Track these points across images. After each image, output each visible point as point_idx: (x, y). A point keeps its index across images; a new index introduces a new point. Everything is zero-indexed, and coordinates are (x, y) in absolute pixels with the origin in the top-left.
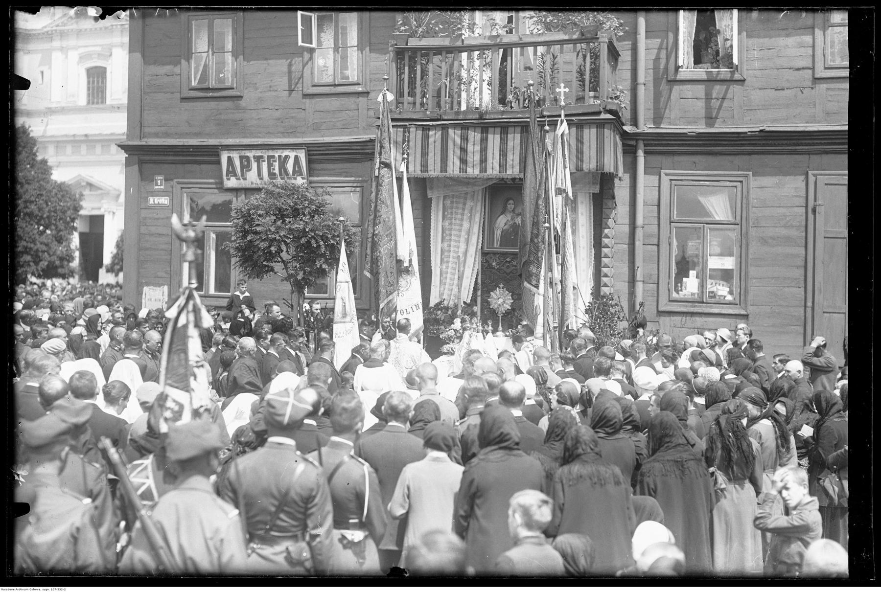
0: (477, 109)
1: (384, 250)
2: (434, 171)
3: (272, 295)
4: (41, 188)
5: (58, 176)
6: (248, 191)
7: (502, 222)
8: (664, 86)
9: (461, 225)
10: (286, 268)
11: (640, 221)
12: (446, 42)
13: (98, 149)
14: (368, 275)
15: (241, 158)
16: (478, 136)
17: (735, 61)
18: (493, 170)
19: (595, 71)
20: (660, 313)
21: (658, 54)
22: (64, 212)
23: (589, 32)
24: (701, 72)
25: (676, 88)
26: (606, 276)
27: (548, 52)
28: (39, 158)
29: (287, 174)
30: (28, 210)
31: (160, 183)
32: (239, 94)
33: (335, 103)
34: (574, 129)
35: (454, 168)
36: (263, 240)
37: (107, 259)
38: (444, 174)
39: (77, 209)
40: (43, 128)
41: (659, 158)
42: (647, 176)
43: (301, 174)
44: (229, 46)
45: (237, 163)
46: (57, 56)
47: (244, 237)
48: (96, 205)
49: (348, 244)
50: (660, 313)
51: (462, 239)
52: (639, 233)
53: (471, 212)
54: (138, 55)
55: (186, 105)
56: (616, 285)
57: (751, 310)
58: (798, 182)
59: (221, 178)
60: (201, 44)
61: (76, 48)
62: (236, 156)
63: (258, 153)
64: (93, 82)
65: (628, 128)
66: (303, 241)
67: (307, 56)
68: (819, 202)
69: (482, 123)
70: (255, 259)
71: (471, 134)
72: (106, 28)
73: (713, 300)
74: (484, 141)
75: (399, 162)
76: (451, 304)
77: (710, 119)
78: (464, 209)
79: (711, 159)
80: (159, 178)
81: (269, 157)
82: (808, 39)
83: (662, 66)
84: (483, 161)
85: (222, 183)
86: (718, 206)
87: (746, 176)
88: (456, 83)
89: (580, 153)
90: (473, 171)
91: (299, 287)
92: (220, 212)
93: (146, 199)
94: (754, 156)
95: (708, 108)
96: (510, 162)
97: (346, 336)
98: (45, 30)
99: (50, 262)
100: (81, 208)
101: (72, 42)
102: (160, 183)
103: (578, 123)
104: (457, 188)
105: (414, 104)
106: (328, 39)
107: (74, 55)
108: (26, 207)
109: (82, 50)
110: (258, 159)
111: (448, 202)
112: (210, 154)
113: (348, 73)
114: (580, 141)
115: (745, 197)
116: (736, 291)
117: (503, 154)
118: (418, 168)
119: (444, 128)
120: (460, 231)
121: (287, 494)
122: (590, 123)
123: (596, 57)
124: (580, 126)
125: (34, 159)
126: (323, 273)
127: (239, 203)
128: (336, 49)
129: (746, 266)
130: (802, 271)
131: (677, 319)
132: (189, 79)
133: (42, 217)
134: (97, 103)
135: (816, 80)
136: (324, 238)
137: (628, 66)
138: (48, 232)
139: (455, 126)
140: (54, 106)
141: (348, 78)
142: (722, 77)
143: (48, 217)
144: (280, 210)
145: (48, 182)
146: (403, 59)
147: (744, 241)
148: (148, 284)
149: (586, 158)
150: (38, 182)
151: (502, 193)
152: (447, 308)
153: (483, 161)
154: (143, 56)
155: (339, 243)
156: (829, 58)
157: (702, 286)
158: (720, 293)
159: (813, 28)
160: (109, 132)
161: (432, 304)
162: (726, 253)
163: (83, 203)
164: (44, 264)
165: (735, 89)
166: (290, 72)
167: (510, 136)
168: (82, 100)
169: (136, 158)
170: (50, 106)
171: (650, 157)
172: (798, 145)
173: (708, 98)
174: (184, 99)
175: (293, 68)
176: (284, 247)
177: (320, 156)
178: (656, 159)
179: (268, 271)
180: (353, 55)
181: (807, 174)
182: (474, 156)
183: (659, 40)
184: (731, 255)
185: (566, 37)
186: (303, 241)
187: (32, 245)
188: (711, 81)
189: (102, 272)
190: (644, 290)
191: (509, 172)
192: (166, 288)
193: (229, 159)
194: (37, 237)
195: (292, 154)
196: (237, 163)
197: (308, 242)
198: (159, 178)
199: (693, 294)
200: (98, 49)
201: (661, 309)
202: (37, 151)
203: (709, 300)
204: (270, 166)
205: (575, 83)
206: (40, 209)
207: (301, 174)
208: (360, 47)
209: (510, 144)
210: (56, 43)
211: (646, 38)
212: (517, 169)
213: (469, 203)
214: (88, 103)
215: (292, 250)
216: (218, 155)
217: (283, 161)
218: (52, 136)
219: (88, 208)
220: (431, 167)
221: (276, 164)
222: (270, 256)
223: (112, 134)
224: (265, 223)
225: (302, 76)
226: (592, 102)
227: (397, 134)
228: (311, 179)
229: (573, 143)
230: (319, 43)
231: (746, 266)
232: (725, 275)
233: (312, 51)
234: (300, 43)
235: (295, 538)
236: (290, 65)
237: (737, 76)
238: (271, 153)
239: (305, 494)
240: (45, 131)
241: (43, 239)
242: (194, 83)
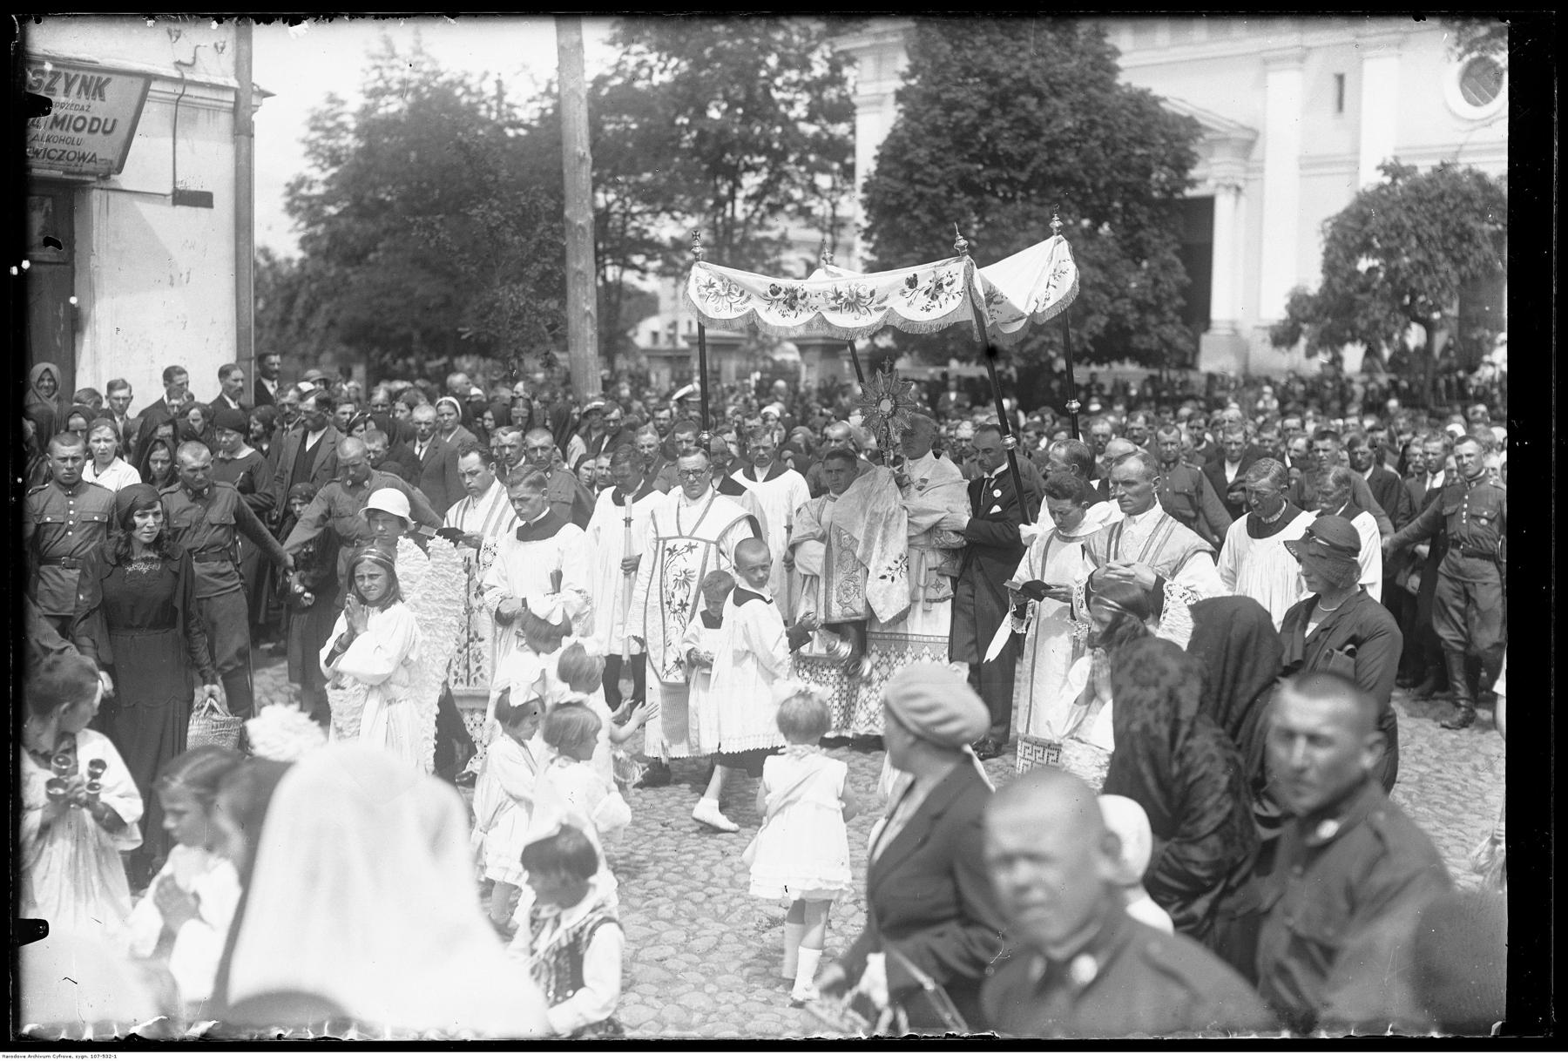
30: (1057, 169)
108: (1052, 160)
150: (1082, 87)
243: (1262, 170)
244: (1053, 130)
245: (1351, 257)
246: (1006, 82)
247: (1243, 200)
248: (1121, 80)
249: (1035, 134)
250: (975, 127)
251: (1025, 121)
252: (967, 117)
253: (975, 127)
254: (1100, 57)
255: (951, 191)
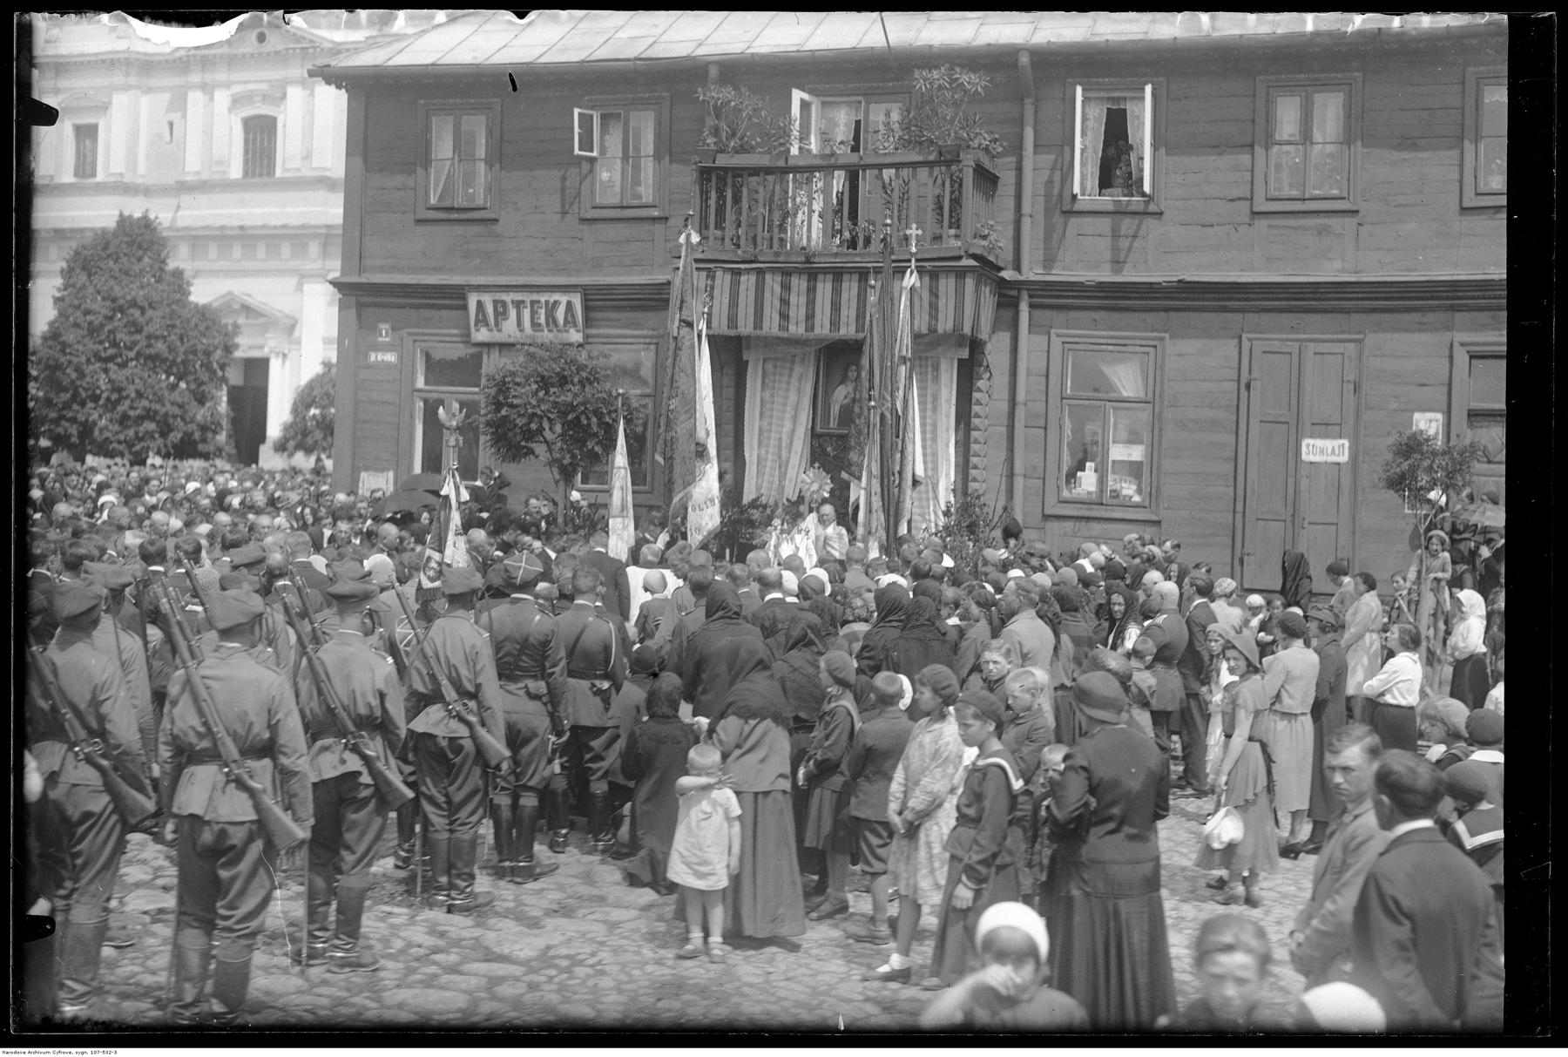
0: (803, 248)
1: (680, 429)
2: (745, 327)
3: (532, 485)
4: (173, 315)
5: (202, 293)
6: (503, 346)
7: (841, 394)
8: (1057, 219)
9: (786, 398)
10: (550, 450)
11: (1021, 396)
12: (765, 161)
13: (261, 252)
14: (659, 459)
15: (495, 302)
16: (804, 284)
17: (1147, 188)
18: (822, 328)
19: (956, 202)
20: (1046, 517)
21: (1051, 175)
22: (208, 353)
23: (949, 152)
24: (1107, 201)
25: (1074, 221)
26: (976, 467)
27: (897, 175)
28: (172, 265)
29: (555, 323)
30: (152, 351)
31: (385, 333)
32: (493, 216)
33: (622, 230)
34: (927, 279)
35: (771, 325)
36: (520, 415)
37: (274, 430)
38: (758, 332)
39: (228, 349)
40: (171, 215)
41: (1049, 313)
42: (1033, 337)
43: (575, 325)
44: (481, 152)
45: (490, 309)
46: (196, 98)
47: (498, 410)
48: (258, 342)
49: (628, 421)
50: (1046, 517)
51: (788, 416)
52: (1020, 412)
53: (800, 381)
54: (359, 160)
55: (421, 229)
56: (988, 483)
57: (1163, 515)
58: (1230, 347)
59: (468, 328)
60: (443, 148)
61: (227, 85)
62: (488, 299)
63: (519, 297)
64: (254, 141)
65: (1007, 274)
66: (570, 417)
67: (586, 166)
68: (1254, 375)
69: (811, 269)
70: (512, 439)
71: (795, 281)
72: (277, 53)
73: (1115, 501)
74: (811, 290)
75: (703, 313)
76: (771, 502)
77: (1117, 263)
78: (790, 376)
79: (1116, 316)
80: (384, 327)
81: (533, 303)
82: (1245, 159)
83: (1056, 192)
84: (810, 317)
85: (468, 335)
86: (1126, 379)
87: (1161, 339)
88: (777, 215)
89: (934, 308)
90: (797, 329)
91: (567, 475)
92: (463, 370)
93: (367, 356)
94: (1173, 315)
95: (1115, 249)
96: (843, 319)
97: (619, 538)
98: (177, 55)
99: (185, 433)
100: (237, 346)
101: (221, 75)
102: (385, 333)
103: (932, 271)
104: (782, 349)
105: (723, 239)
106: (614, 143)
107: (222, 98)
108: (149, 346)
109: (237, 89)
110: (518, 305)
111: (770, 366)
112: (454, 297)
113: (642, 189)
114: (934, 293)
115: (1159, 367)
116: (1146, 488)
117: (836, 307)
118: (725, 322)
119: (760, 273)
120: (785, 405)
121: (527, 639)
122: (947, 271)
123: (958, 184)
124: (934, 275)
125: (162, 270)
126: (594, 458)
127: (492, 364)
128: (625, 158)
129: (1159, 458)
130: (1231, 466)
131: (1069, 525)
132: (427, 193)
133: (174, 362)
134: (261, 175)
135: (1255, 214)
136: (597, 412)
137: (1012, 191)
138: (183, 385)
139: (773, 270)
140: (189, 178)
141: (640, 197)
142: (1133, 208)
143: (183, 362)
144: (543, 377)
145: (184, 306)
146: (709, 180)
147: (1156, 426)
148: (366, 469)
149: (941, 316)
150: (169, 305)
151: (839, 357)
152: (765, 507)
153: (810, 317)
154: (365, 162)
155: (615, 421)
156: (1272, 185)
157: (1102, 482)
158: (1125, 492)
159: (1252, 146)
160: (279, 223)
161: (746, 499)
162: (1133, 439)
163: (239, 340)
164: (175, 436)
165: (1150, 222)
166: (563, 189)
167: (845, 285)
168: (236, 171)
169: (353, 300)
170: (182, 178)
171: (1036, 313)
172: (1229, 299)
173: (1115, 235)
174: (419, 221)
175: (568, 184)
176: (546, 425)
177: (598, 301)
178: (1044, 316)
179: (526, 454)
180: (648, 168)
181: (1240, 338)
182: (798, 310)
183: (1053, 157)
184: (1140, 442)
185: (920, 158)
186: (570, 417)
187: (158, 407)
188: (1119, 212)
189: (265, 451)
190: (1025, 486)
191: (843, 331)
192: (391, 474)
193: (479, 303)
194: (166, 393)
195: (563, 299)
196: (490, 309)
197: (577, 418)
198: (384, 327)
199: (1089, 493)
200: (264, 87)
201: (1047, 512)
202: (167, 256)
203: (1110, 502)
204: (533, 313)
205: (930, 216)
206: (170, 350)
207: (575, 325)
208: (658, 157)
209: (845, 295)
210: (195, 78)
211: (1035, 153)
212: (852, 328)
213: (798, 369)
214: (246, 174)
215: (558, 428)
216: (464, 298)
217: (551, 308)
218: (186, 228)
219: (246, 346)
220: (741, 323)
221: (542, 312)
222: (530, 435)
223: (284, 226)
224: (524, 394)
225: (579, 194)
226: (952, 244)
227: (700, 279)
228: (590, 331)
229: (926, 295)
230: (603, 151)
231: (1159, 458)
232: (1134, 470)
233: (592, 160)
234: (577, 151)
235: (535, 677)
236: (564, 179)
237: (1152, 208)
238: (535, 297)
239: (542, 638)
240: (174, 219)
241: (176, 396)
242: (433, 201)
243: (299, 343)
244: (148, 330)
245: (308, 407)
246: (122, 302)
247: (288, 363)
248: (192, 298)
249: (139, 331)
250: (102, 326)
251: (134, 323)
252: (96, 320)
253: (102, 326)
254: (180, 286)
255: (88, 360)
